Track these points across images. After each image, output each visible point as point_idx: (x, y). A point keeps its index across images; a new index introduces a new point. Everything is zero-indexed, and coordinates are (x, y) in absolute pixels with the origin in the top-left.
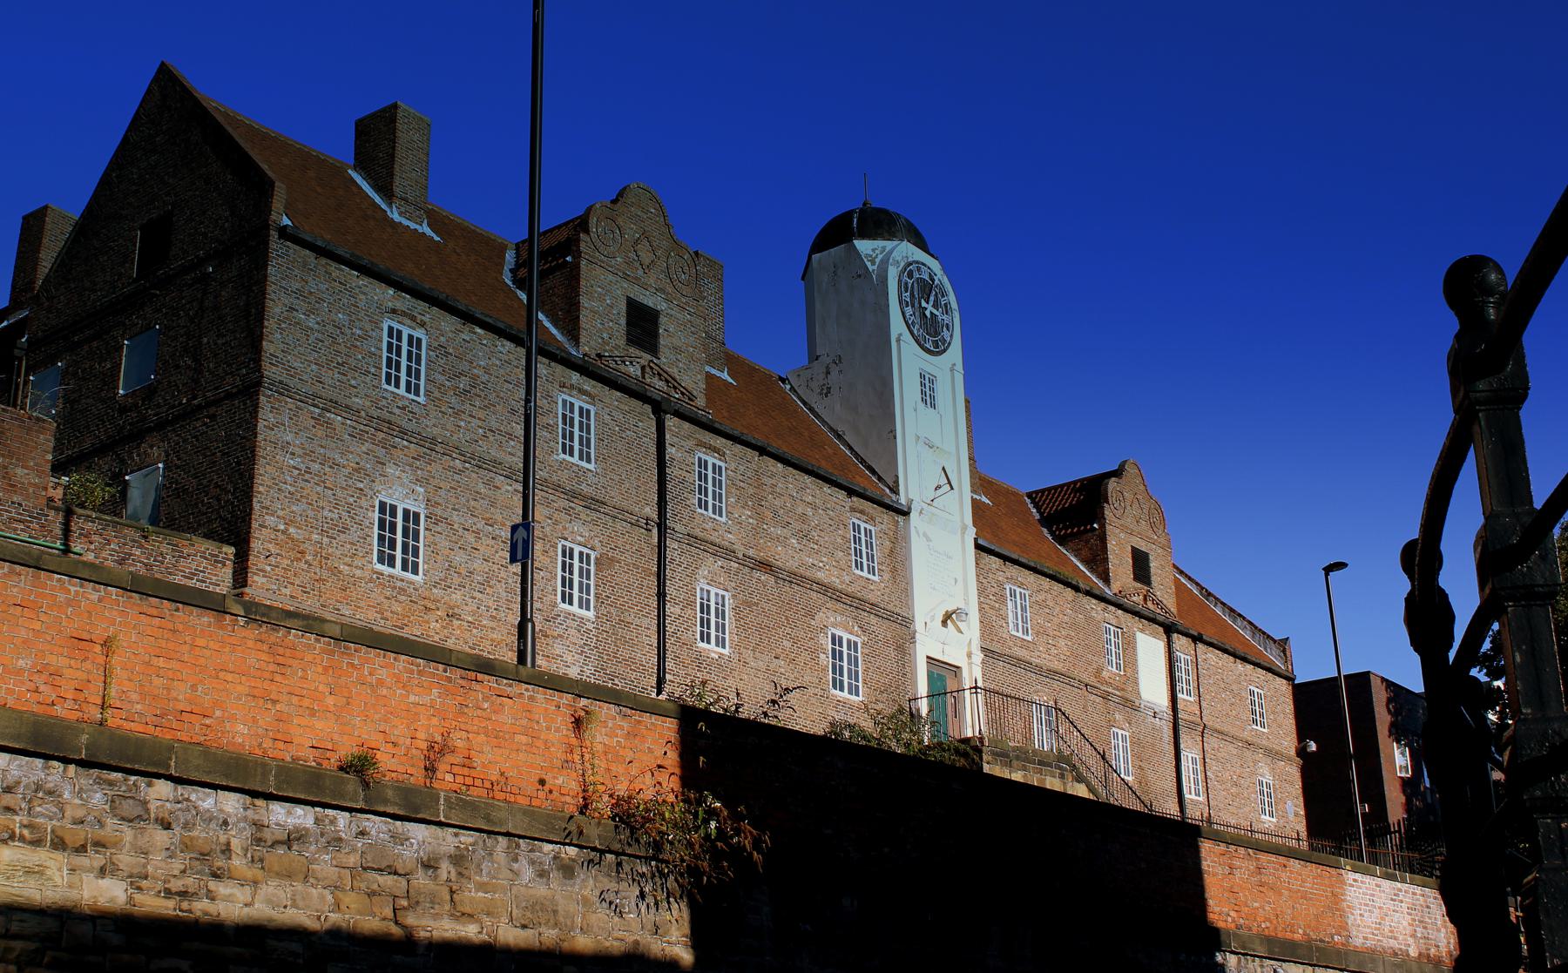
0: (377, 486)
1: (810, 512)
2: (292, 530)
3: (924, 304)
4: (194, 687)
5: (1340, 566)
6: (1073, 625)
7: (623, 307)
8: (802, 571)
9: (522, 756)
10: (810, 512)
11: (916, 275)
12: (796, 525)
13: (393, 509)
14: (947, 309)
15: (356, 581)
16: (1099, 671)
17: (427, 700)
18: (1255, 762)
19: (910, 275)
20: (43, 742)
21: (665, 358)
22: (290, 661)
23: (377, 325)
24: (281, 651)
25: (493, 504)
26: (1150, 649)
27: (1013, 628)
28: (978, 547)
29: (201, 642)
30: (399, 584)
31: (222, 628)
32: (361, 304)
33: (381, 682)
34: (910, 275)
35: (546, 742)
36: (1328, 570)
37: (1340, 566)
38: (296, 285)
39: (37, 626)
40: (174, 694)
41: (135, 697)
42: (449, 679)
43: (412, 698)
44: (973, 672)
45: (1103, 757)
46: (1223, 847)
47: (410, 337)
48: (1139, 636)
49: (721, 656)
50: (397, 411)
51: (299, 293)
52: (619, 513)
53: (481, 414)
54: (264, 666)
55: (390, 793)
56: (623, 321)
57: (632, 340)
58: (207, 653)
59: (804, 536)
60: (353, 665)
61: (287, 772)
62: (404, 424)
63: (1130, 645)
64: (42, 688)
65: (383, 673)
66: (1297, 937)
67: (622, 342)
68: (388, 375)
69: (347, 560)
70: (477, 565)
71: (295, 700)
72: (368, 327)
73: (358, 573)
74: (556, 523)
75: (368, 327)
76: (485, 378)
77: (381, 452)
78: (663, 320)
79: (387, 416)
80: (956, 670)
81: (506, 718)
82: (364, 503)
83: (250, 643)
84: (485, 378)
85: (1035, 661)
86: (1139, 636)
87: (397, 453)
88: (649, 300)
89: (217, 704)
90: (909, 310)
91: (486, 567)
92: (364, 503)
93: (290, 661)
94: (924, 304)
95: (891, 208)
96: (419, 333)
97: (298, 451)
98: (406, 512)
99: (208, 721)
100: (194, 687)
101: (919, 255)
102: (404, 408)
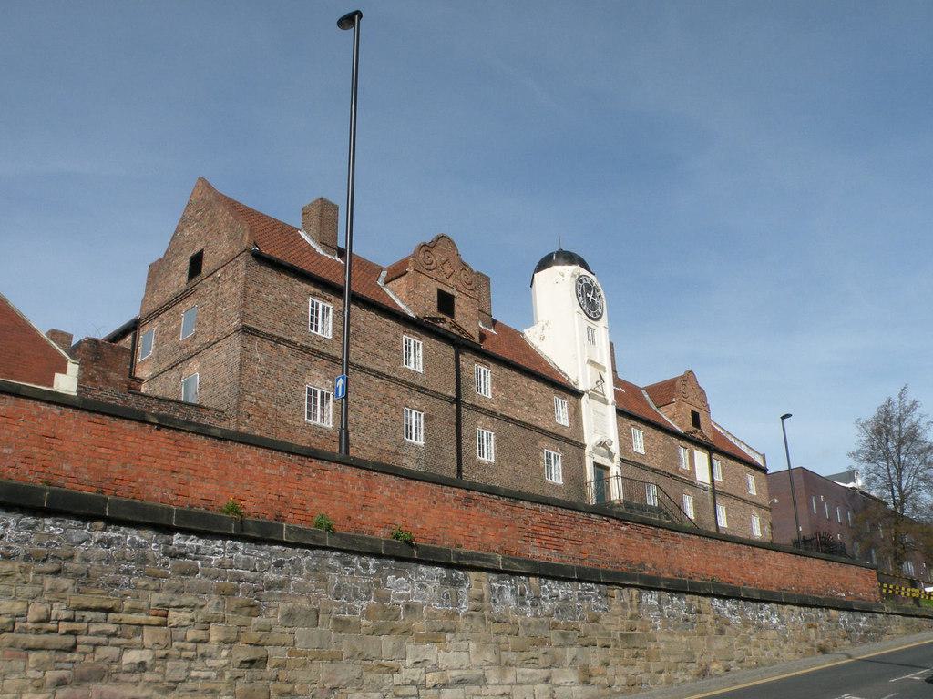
0: (306, 380)
1: (533, 393)
2: (260, 402)
3: (588, 295)
4: (124, 465)
5: (788, 416)
6: (665, 447)
7: (436, 293)
8: (530, 422)
9: (336, 503)
10: (533, 393)
11: (584, 282)
12: (527, 400)
13: (315, 392)
14: (600, 298)
15: (296, 428)
16: (677, 468)
17: (276, 472)
18: (751, 509)
19: (581, 282)
20: (931, 618)
21: (458, 318)
22: (188, 450)
23: (305, 300)
24: (183, 444)
25: (369, 389)
26: (701, 457)
27: (639, 446)
28: (619, 412)
29: (129, 438)
30: (319, 429)
31: (144, 431)
32: (297, 290)
33: (247, 463)
34: (581, 282)
35: (352, 495)
36: (783, 418)
37: (788, 416)
38: (261, 280)
39: (17, 428)
40: (110, 469)
41: (85, 470)
42: (291, 460)
43: (267, 471)
44: (615, 469)
45: (679, 508)
46: (736, 545)
47: (323, 307)
48: (695, 451)
49: (490, 463)
50: (317, 343)
51: (263, 284)
52: (435, 395)
53: (361, 345)
54: (171, 452)
55: (251, 525)
56: (436, 300)
57: (441, 309)
58: (134, 445)
59: (532, 405)
60: (230, 453)
61: (185, 515)
62: (320, 349)
63: (692, 456)
64: (19, 465)
65: (249, 457)
66: (774, 589)
67: (436, 311)
68: (312, 326)
69: (291, 417)
70: (361, 419)
71: (191, 472)
72: (300, 301)
73: (297, 424)
74: (402, 399)
75: (300, 301)
76: (363, 327)
77: (308, 363)
78: (456, 301)
79: (311, 346)
80: (607, 468)
81: (326, 482)
82: (299, 388)
83: (162, 439)
84: (363, 327)
85: (646, 464)
86: (695, 451)
87: (317, 364)
88: (449, 291)
89: (140, 475)
90: (581, 298)
91: (366, 420)
92: (299, 388)
93: (188, 450)
94: (588, 295)
95: (573, 251)
96: (327, 305)
97: (263, 363)
98: (322, 394)
99: (133, 485)
100: (124, 465)
101: (584, 272)
102: (320, 342)
